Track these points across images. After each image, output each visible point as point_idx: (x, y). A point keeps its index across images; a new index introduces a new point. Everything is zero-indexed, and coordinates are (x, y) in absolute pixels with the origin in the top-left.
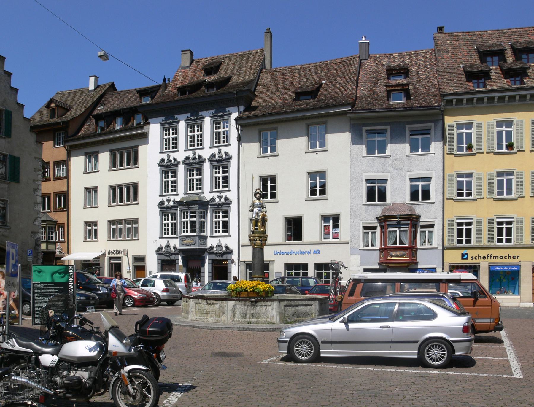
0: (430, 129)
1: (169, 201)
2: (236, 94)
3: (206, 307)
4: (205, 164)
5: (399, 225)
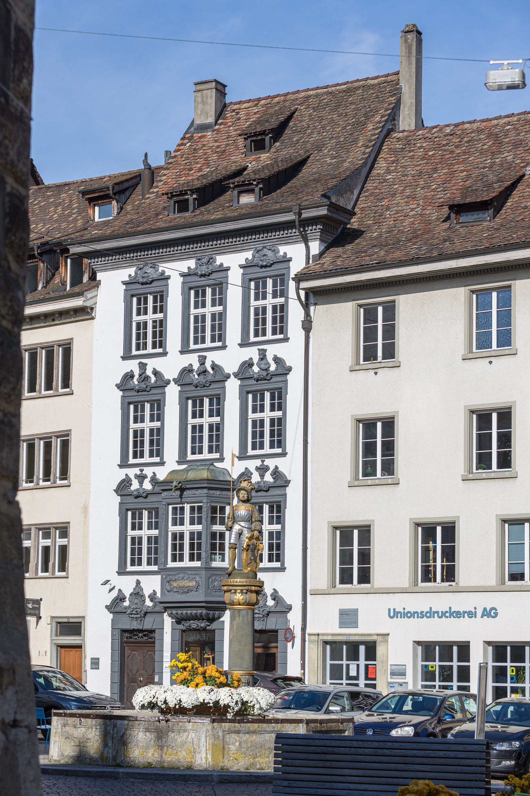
1: (141, 478)
4: (227, 384)
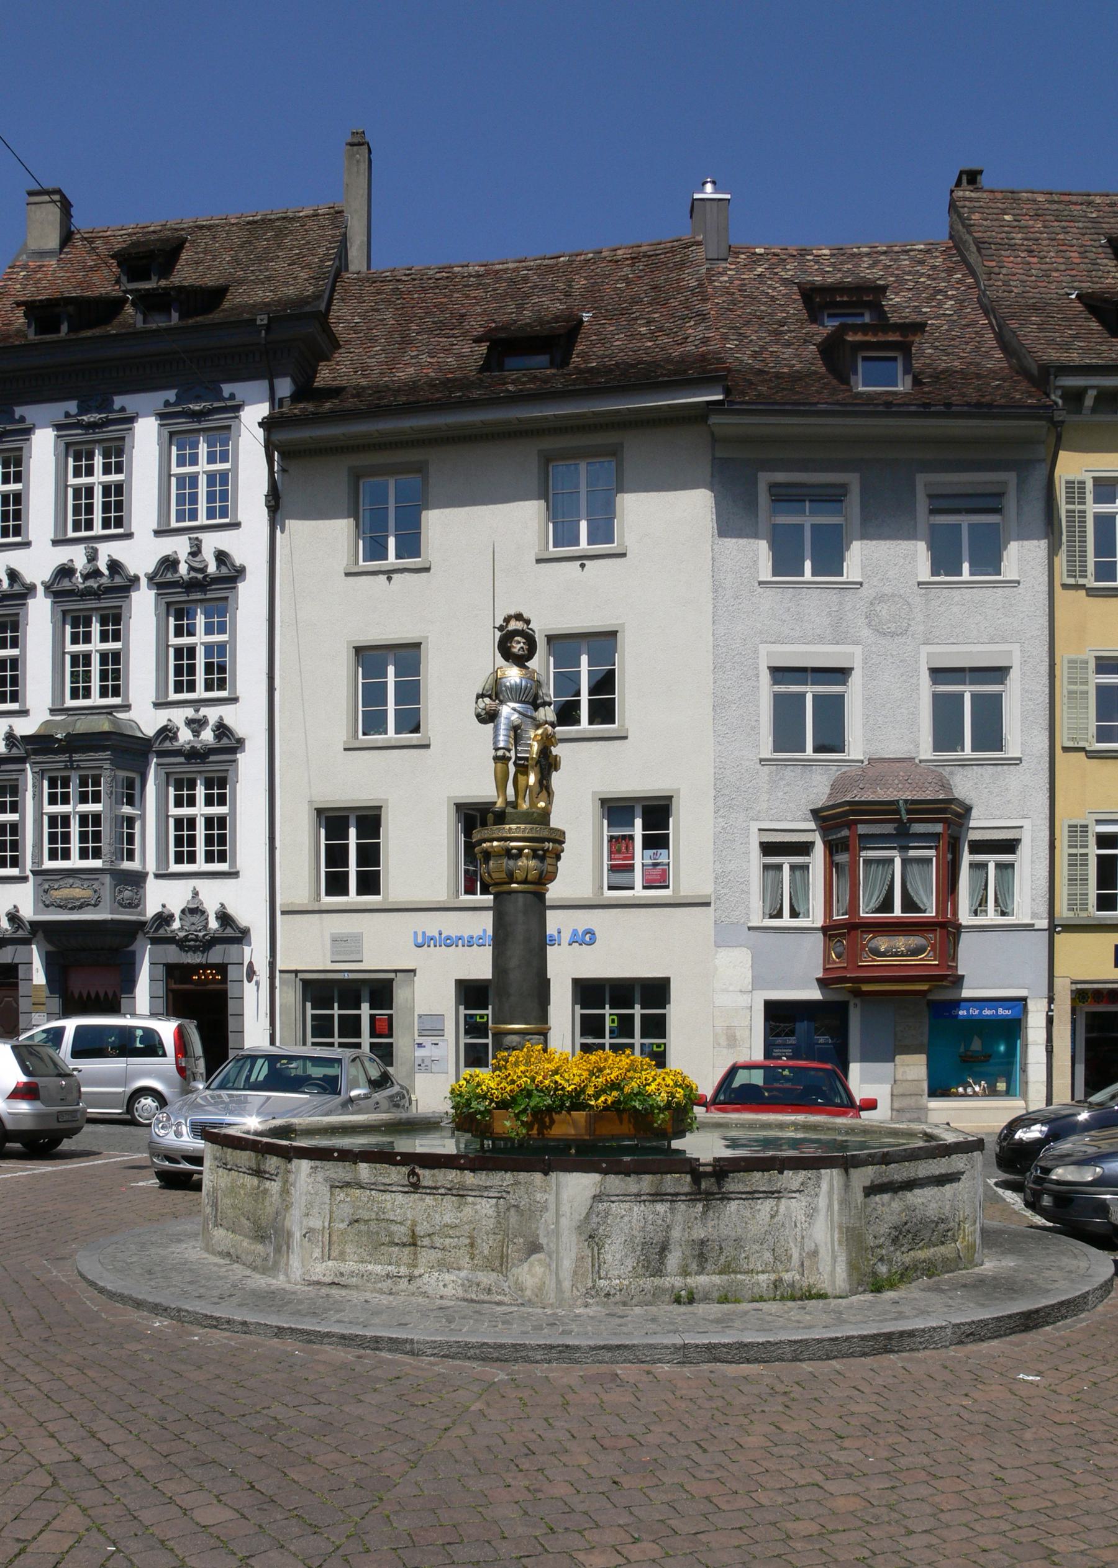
0: (1001, 495)
2: (268, 328)
3: (403, 1208)
5: (902, 838)
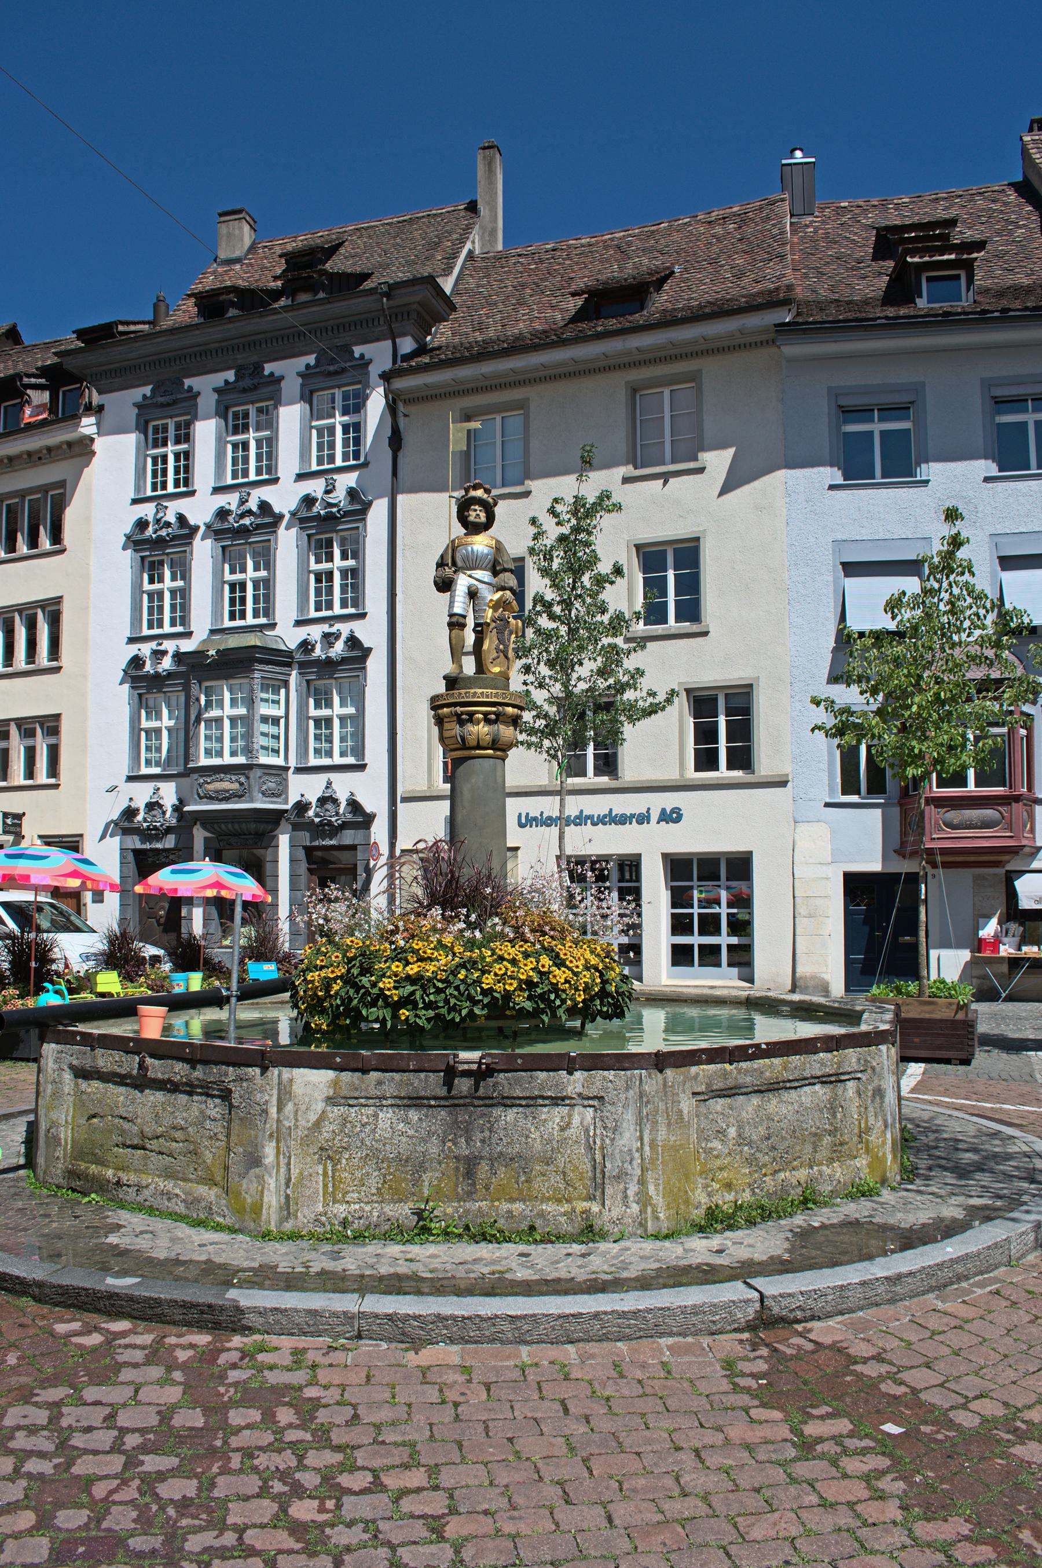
1: (158, 654)
